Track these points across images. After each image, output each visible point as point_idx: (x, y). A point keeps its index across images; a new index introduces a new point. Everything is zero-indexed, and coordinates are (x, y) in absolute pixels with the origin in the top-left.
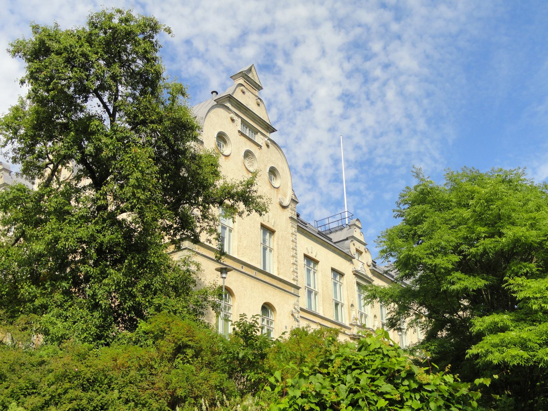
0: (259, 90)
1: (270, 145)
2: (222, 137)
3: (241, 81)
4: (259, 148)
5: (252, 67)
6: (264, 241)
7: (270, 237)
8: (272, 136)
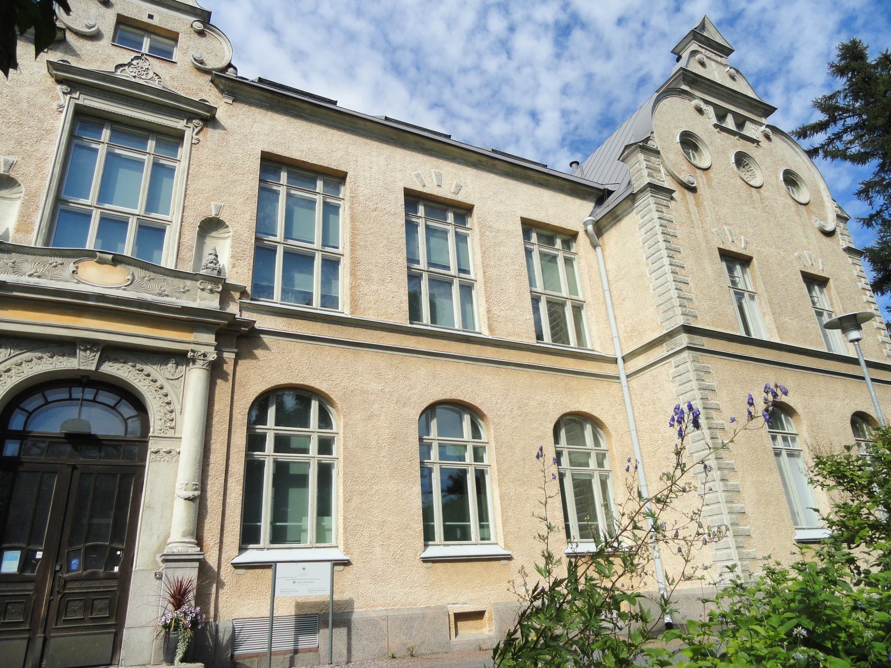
0: (728, 56)
1: (772, 136)
2: (689, 142)
3: (694, 46)
4: (755, 144)
5: (704, 18)
6: (734, 283)
7: (743, 273)
8: (771, 120)
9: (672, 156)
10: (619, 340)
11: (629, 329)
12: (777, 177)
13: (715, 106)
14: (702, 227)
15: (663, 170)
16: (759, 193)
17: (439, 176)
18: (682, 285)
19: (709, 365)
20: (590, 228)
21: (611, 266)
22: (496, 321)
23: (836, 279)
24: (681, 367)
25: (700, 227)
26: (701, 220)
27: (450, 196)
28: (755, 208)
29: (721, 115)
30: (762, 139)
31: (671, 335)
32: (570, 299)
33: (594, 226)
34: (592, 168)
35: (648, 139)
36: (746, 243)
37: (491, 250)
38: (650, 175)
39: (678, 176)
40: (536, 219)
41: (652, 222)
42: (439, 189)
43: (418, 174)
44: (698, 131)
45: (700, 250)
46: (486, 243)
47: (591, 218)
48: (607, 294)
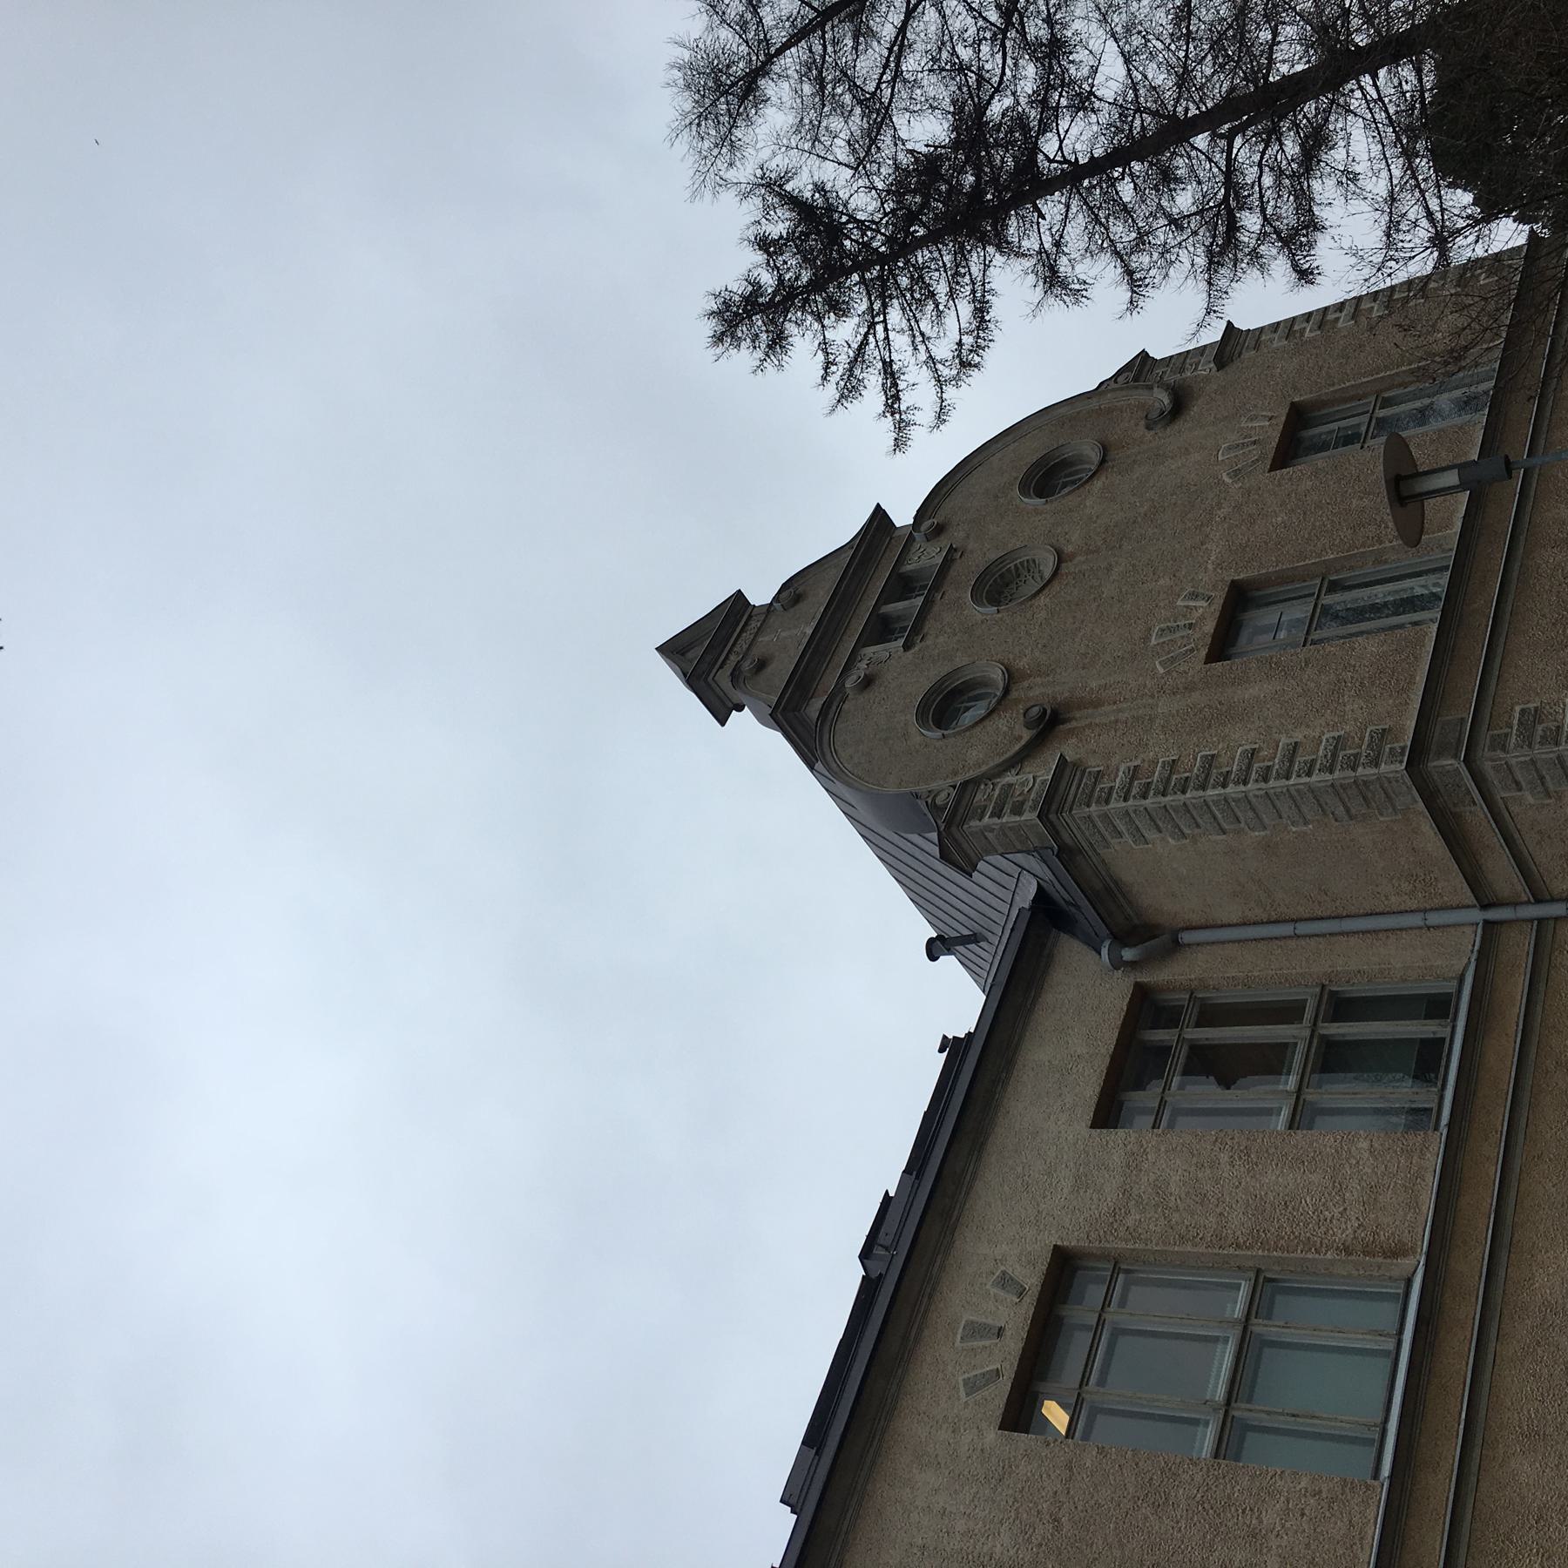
9: (974, 755)
10: (1431, 909)
11: (1406, 886)
12: (1037, 512)
13: (864, 641)
14: (1152, 696)
15: (1009, 778)
16: (1072, 556)
17: (975, 1330)
18: (1299, 759)
19: (1518, 709)
20: (1128, 954)
21: (1232, 912)
22: (1375, 1233)
23: (1295, 388)
24: (1520, 778)
25: (1150, 701)
26: (1134, 699)
27: (1027, 1308)
28: (1109, 569)
29: (881, 629)
30: (944, 542)
31: (1429, 796)
32: (1315, 1024)
33: (1126, 945)
34: (972, 913)
35: (935, 808)
36: (1194, 596)
37: (1176, 1217)
38: (1018, 810)
39: (1023, 742)
40: (1098, 1089)
41: (1133, 815)
42: (1008, 1333)
43: (966, 1382)
44: (919, 684)
45: (1210, 707)
46: (1158, 1229)
47: (1105, 952)
48: (1303, 928)
